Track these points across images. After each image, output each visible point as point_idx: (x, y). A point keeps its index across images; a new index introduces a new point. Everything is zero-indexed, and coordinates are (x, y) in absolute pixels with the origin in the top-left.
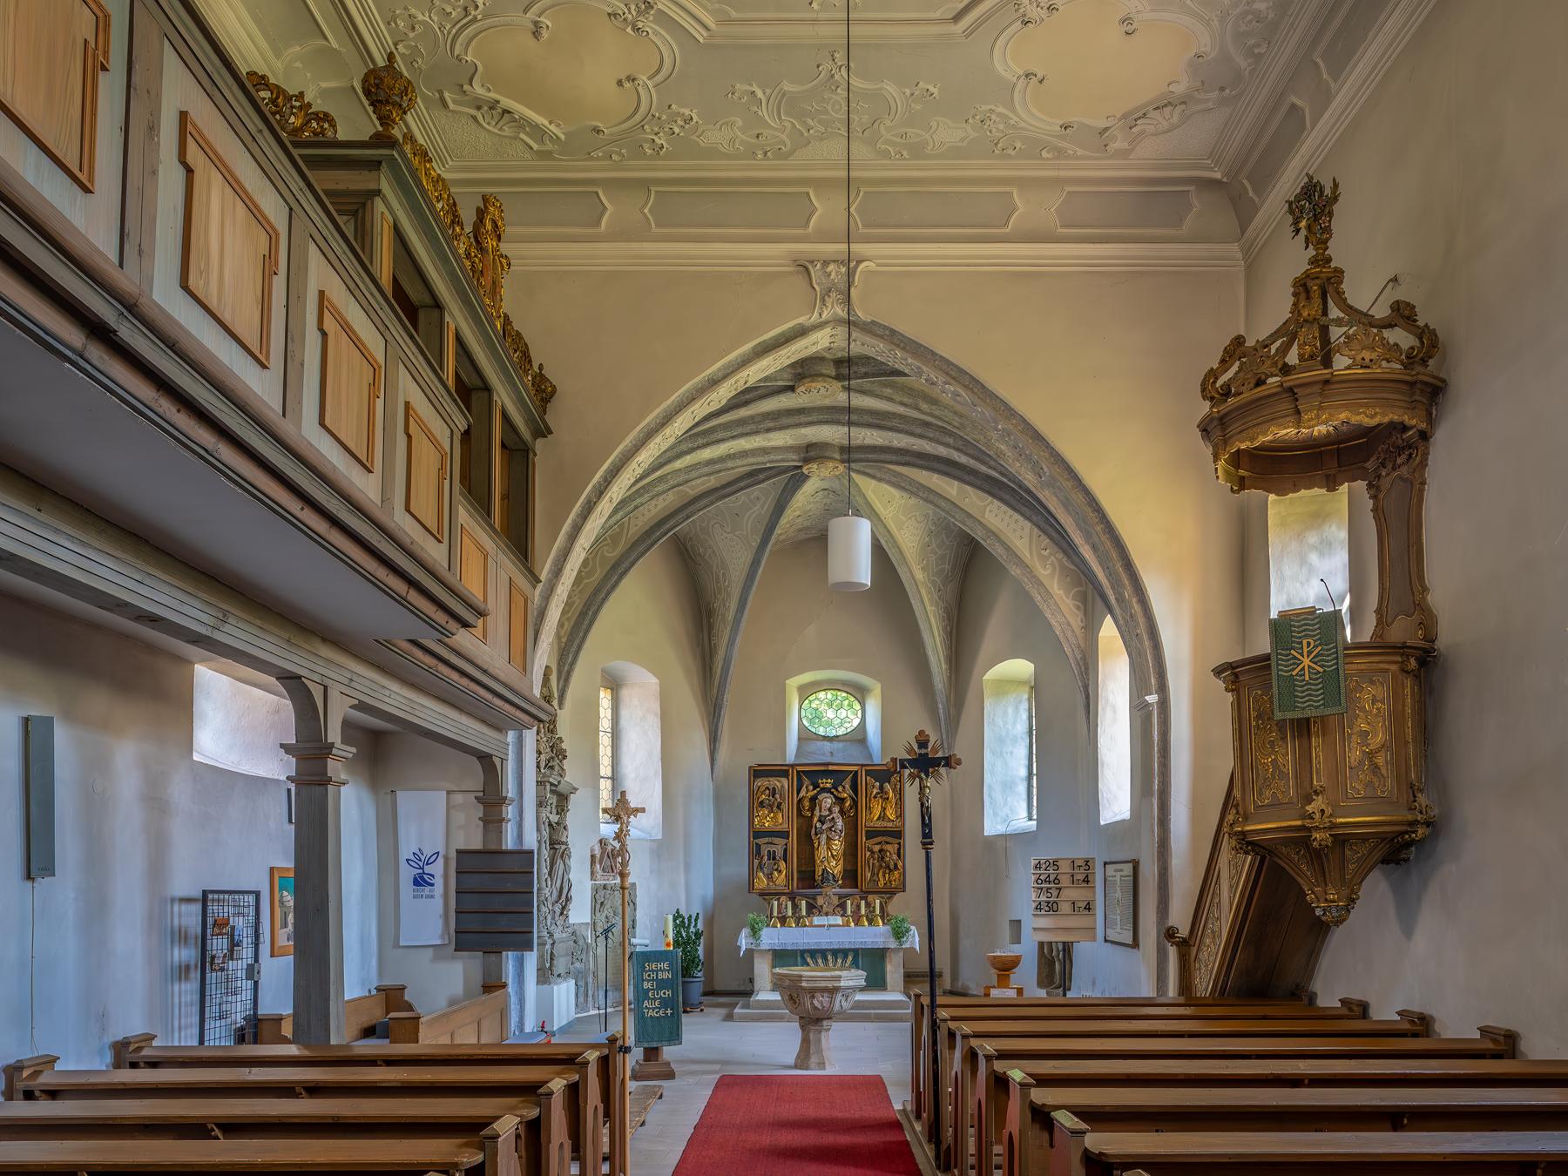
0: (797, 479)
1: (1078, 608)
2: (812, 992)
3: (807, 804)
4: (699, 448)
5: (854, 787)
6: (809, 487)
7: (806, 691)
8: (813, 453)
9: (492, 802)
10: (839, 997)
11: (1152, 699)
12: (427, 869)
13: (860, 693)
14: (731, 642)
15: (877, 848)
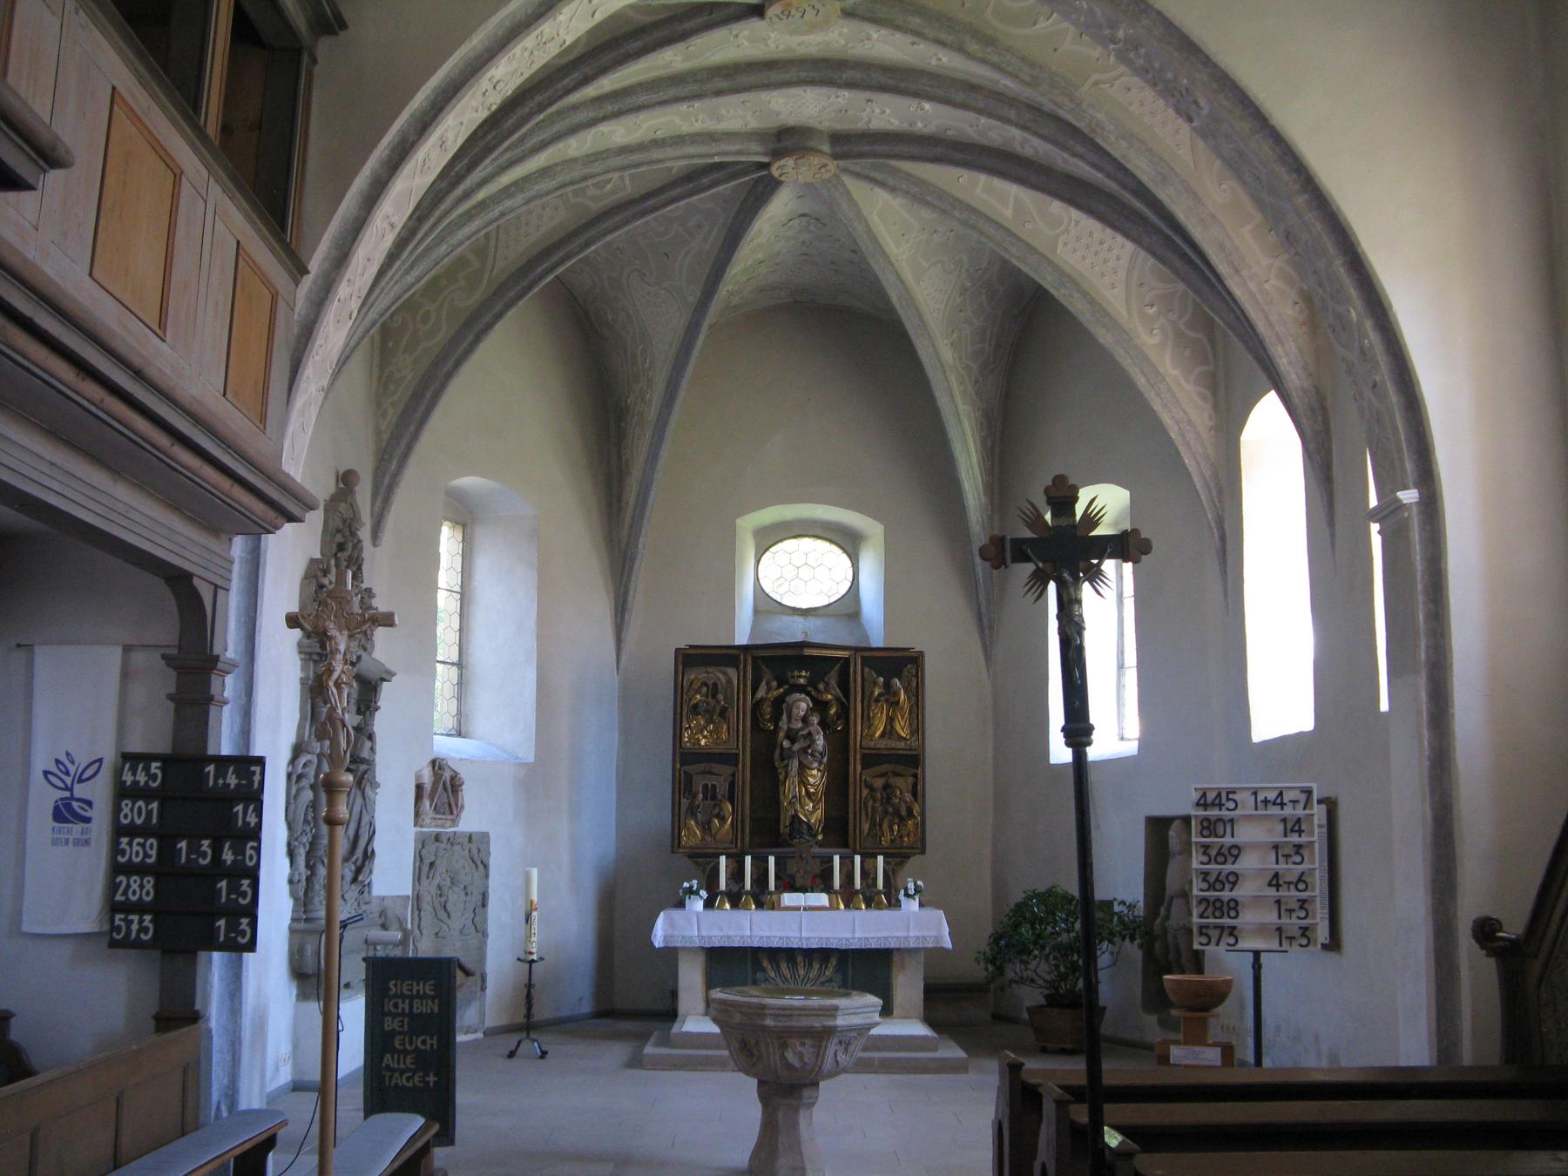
0: (763, 188)
1: (1204, 398)
2: (784, 1037)
3: (767, 709)
4: (605, 118)
5: (844, 685)
6: (780, 206)
7: (768, 538)
8: (787, 140)
9: (194, 670)
10: (832, 1046)
11: (1409, 496)
12: (79, 790)
13: (849, 541)
14: (653, 456)
15: (879, 783)
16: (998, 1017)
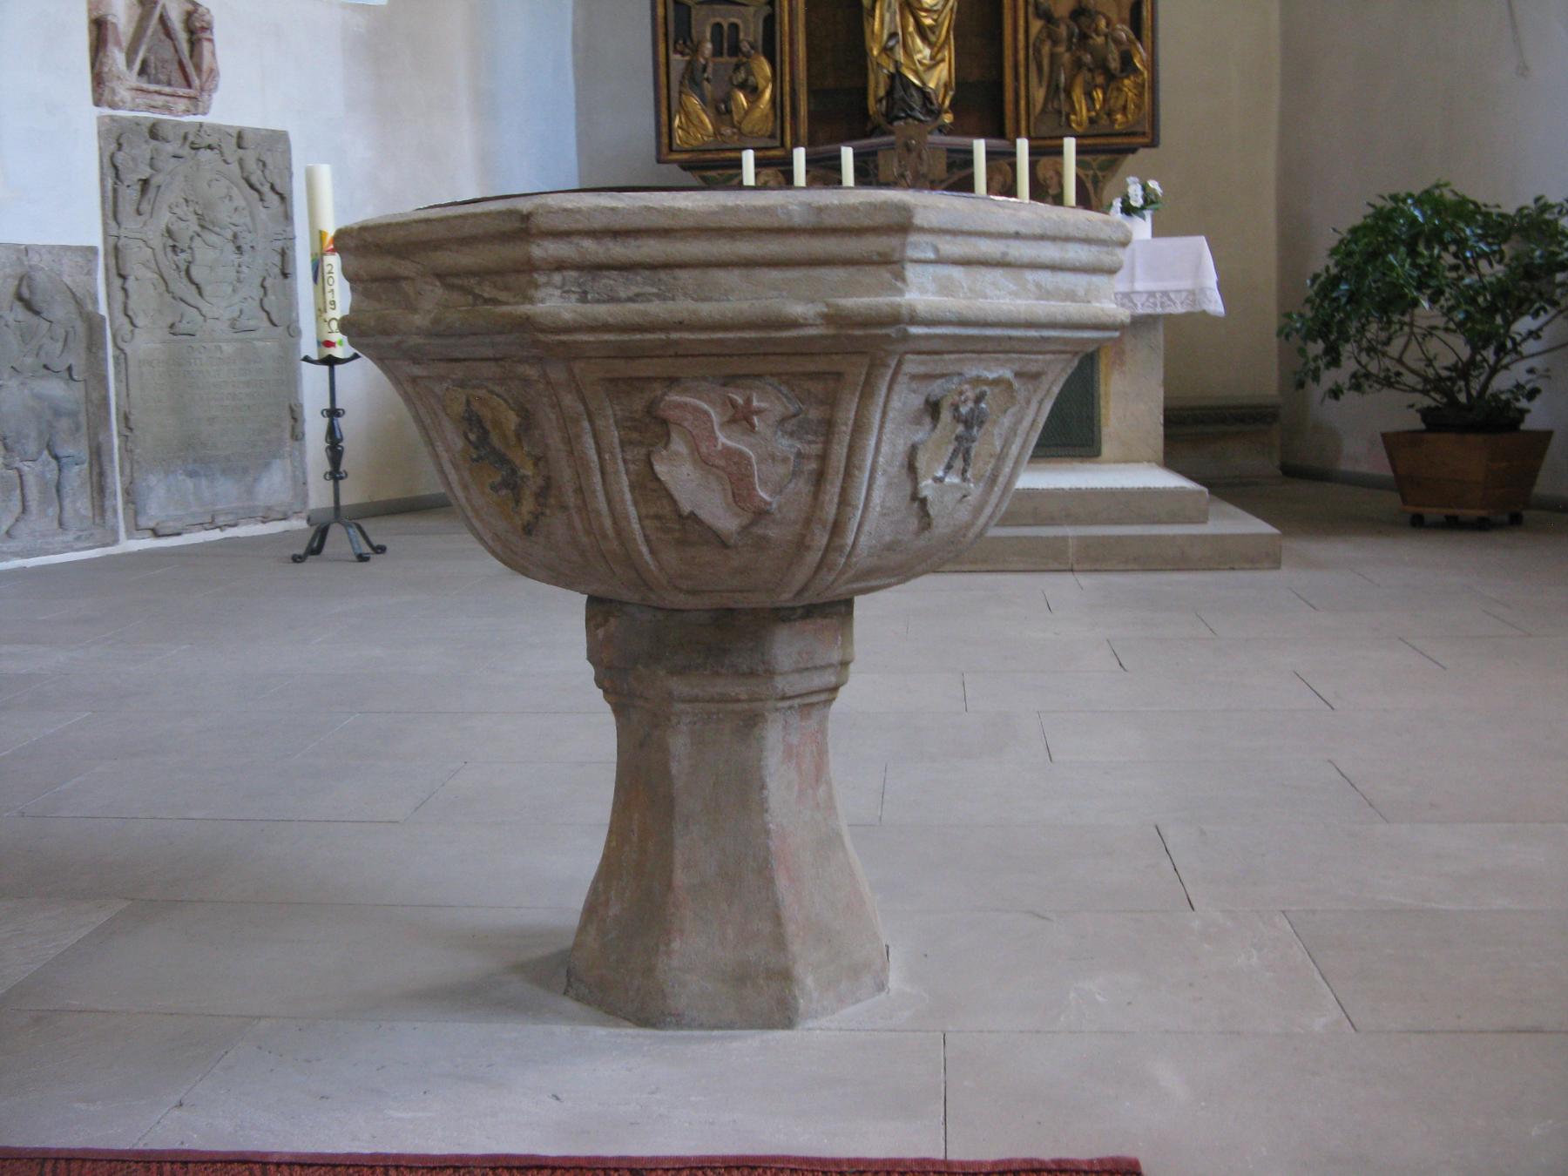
10: (890, 430)
16: (1291, 472)
